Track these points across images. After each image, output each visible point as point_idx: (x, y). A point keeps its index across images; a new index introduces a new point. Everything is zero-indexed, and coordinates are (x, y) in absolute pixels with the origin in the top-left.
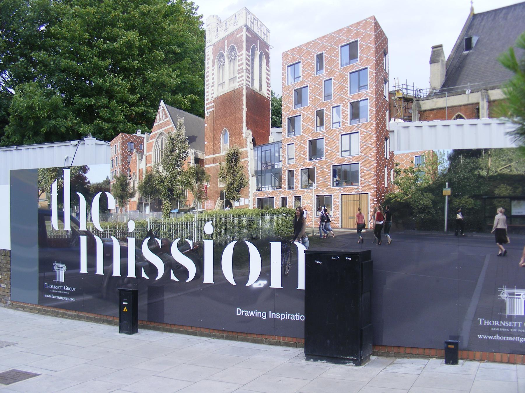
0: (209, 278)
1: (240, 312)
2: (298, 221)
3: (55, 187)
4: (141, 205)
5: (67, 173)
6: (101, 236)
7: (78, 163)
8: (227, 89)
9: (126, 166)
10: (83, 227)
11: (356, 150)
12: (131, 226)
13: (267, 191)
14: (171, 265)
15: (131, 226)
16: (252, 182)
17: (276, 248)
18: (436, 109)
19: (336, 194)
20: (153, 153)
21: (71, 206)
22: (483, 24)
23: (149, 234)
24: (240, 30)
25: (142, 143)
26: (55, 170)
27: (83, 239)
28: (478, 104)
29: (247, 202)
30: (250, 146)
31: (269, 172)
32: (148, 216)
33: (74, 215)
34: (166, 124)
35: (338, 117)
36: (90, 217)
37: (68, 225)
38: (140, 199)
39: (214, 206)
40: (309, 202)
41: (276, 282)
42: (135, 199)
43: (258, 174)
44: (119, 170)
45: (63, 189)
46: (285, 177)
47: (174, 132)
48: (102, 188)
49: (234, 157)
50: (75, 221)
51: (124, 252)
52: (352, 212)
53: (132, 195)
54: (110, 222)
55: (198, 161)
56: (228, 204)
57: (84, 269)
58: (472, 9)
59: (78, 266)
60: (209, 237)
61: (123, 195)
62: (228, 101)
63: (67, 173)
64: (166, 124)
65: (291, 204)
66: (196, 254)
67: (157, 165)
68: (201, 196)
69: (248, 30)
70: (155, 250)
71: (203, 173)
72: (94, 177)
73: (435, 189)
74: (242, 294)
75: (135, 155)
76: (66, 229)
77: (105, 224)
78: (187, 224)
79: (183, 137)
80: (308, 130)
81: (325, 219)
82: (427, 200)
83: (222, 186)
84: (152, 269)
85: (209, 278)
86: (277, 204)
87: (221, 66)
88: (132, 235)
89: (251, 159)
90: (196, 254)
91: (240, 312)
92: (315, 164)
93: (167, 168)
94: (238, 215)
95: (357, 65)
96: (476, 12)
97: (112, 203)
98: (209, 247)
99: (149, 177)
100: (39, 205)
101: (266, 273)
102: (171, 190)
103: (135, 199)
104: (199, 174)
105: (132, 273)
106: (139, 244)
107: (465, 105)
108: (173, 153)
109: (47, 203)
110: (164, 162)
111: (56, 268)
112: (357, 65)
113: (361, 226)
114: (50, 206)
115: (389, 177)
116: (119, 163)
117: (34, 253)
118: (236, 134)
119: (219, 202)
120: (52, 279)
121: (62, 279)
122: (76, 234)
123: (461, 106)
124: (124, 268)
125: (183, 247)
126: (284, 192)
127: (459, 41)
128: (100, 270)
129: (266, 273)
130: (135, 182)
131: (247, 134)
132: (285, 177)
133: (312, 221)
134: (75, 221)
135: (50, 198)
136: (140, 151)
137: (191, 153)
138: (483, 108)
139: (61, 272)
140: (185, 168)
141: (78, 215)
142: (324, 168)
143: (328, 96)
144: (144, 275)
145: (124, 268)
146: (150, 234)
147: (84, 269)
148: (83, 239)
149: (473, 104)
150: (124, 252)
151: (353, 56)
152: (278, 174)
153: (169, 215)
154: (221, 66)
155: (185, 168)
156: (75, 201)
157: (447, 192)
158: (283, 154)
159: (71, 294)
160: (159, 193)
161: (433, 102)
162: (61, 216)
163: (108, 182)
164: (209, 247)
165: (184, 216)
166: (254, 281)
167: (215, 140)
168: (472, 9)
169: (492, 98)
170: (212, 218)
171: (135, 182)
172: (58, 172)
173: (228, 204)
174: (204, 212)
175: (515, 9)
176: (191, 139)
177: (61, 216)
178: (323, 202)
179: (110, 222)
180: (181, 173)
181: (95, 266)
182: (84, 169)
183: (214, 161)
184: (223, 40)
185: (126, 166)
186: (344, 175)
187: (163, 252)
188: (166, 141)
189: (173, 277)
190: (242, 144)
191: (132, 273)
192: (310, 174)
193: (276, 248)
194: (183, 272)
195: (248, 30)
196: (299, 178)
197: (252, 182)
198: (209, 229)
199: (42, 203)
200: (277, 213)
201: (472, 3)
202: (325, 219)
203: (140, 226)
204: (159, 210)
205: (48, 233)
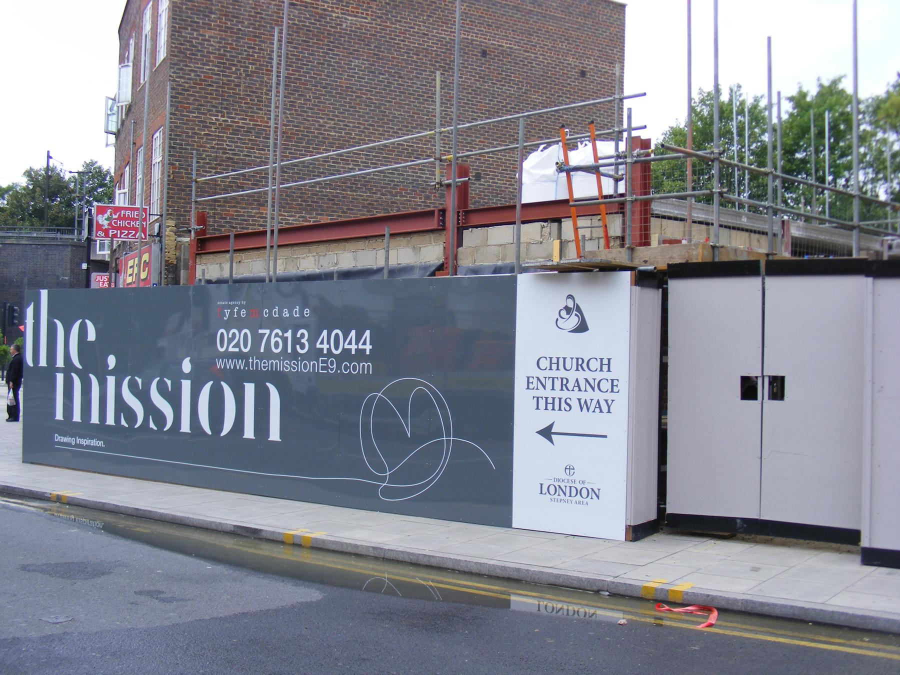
17: (250, 389)
84: (131, 415)
85: (185, 427)
98: (186, 385)
144: (123, 423)
189: (152, 425)
193: (250, 389)
194: (160, 418)
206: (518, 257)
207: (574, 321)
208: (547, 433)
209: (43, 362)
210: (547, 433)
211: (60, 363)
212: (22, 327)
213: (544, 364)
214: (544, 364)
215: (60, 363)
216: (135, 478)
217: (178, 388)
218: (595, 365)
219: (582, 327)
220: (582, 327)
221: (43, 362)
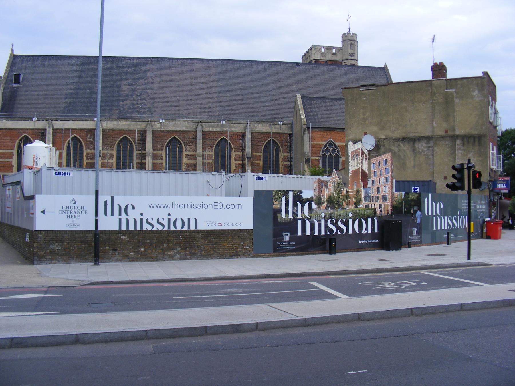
0: (350, 232)
1: (360, 242)
2: (375, 212)
3: (284, 199)
4: (327, 207)
5: (291, 194)
6: (308, 219)
7: (297, 189)
8: (355, 168)
9: (320, 191)
10: (300, 216)
11: (387, 191)
12: (323, 215)
13: (367, 202)
14: (338, 228)
15: (323, 215)
16: (363, 199)
17: (369, 220)
18: (6, 129)
19: (383, 203)
20: (331, 188)
21: (293, 207)
22: (24, 64)
23: (329, 218)
24: (359, 149)
25: (327, 184)
26: (284, 191)
27: (300, 222)
28: (46, 129)
29: (362, 206)
30: (362, 188)
31: (368, 197)
32: (330, 211)
33: (295, 211)
34: (336, 177)
35: (383, 181)
36: (303, 211)
37: (291, 216)
38: (327, 205)
39: (352, 207)
40: (377, 206)
41: (370, 231)
42: (325, 205)
43: (365, 197)
44: (317, 193)
45: (289, 200)
46: (372, 198)
47: (339, 181)
48: (310, 200)
49: (358, 191)
50: (295, 214)
51: (320, 225)
52: (386, 209)
53: (323, 203)
54: (313, 214)
55: (347, 192)
56: (356, 207)
57: (300, 233)
58: (12, 50)
59: (297, 232)
60: (350, 218)
61: (319, 203)
62: (355, 172)
63: (291, 194)
64: (336, 177)
65: (373, 207)
66: (346, 224)
67: (333, 192)
68: (348, 204)
69: (361, 149)
70: (333, 224)
71: (348, 196)
72: (306, 195)
73: (401, 203)
74: (361, 236)
75: (324, 188)
76: (290, 217)
77: (311, 215)
78: (344, 213)
79: (342, 183)
80: (377, 184)
81: (381, 211)
82: (400, 206)
83: (354, 200)
84: (331, 231)
85: (350, 232)
86: (370, 207)
87: (354, 160)
88: (323, 218)
89: (363, 193)
90: (346, 224)
91: (360, 242)
92: (378, 195)
93: (337, 194)
94: (359, 210)
95: (387, 166)
96: (16, 53)
97: (314, 206)
98: (350, 221)
99: (330, 197)
100: (274, 207)
101: (367, 229)
102: (338, 202)
103: (325, 205)
104: (347, 197)
105: (323, 233)
106: (326, 222)
107: (31, 129)
108: (339, 188)
109: (279, 206)
110: (335, 191)
111: (284, 235)
112: (387, 166)
113: (388, 213)
114: (280, 207)
115: (394, 199)
116: (317, 191)
117: (269, 230)
118: (358, 184)
119: (354, 206)
120: (282, 240)
121: (288, 239)
122: (295, 220)
123: (28, 129)
124: (320, 231)
125: (342, 222)
126: (371, 203)
127: (6, 75)
128: (308, 233)
129: (367, 229)
130: (324, 198)
131: (361, 184)
132: (372, 198)
133: (378, 212)
134: (295, 214)
135: (281, 204)
136: (326, 187)
137: (345, 188)
138: (49, 133)
139: (287, 237)
140: (343, 194)
141: (297, 211)
142: (380, 196)
143: (381, 175)
144: (328, 233)
145: (320, 231)
146: (331, 218)
147: (300, 233)
148: (300, 222)
149: (38, 129)
150: (320, 225)
151: (386, 164)
152: (370, 197)
153: (337, 211)
154: (354, 160)
155: (343, 194)
156: (295, 205)
157: (404, 204)
158: (371, 191)
159: (293, 245)
160: (332, 202)
161: (2, 123)
162: (287, 212)
163: (312, 198)
164: (350, 221)
165: (343, 211)
166: (364, 232)
167: (352, 185)
168: (12, 50)
169: (55, 127)
170: (351, 211)
171: (324, 198)
172: (286, 193)
173: (356, 207)
174: (349, 210)
175: (50, 60)
176: (345, 184)
177: (287, 212)
178: (380, 206)
179: (313, 214)
180: (341, 196)
181: (306, 232)
182: (301, 192)
183: (352, 192)
184: (354, 151)
185: (320, 191)
186: (385, 198)
187: (336, 224)
188: (336, 184)
189: (339, 233)
190: (360, 187)
191: (323, 233)
192: (377, 197)
193: (369, 220)
194: (342, 230)
195: (361, 149)
196: (375, 198)
197: (363, 199)
198: (350, 215)
199: (276, 205)
200: (370, 209)
201: (13, 45)
202: (381, 211)
203: (326, 215)
204: (334, 209)
205: (279, 220)
206: (433, 131)
207: (74, 202)
208: (43, 212)
209: (430, 214)
210: (43, 212)
211: (434, 214)
212: (116, 115)
213: (64, 208)
214: (64, 208)
215: (434, 214)
216: (223, 233)
217: (347, 222)
218: (79, 208)
219: (75, 203)
220: (75, 203)
221: (430, 214)
